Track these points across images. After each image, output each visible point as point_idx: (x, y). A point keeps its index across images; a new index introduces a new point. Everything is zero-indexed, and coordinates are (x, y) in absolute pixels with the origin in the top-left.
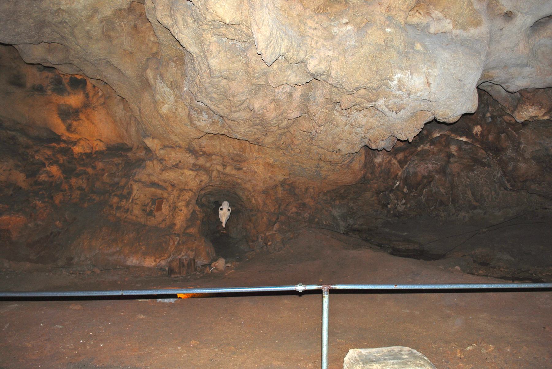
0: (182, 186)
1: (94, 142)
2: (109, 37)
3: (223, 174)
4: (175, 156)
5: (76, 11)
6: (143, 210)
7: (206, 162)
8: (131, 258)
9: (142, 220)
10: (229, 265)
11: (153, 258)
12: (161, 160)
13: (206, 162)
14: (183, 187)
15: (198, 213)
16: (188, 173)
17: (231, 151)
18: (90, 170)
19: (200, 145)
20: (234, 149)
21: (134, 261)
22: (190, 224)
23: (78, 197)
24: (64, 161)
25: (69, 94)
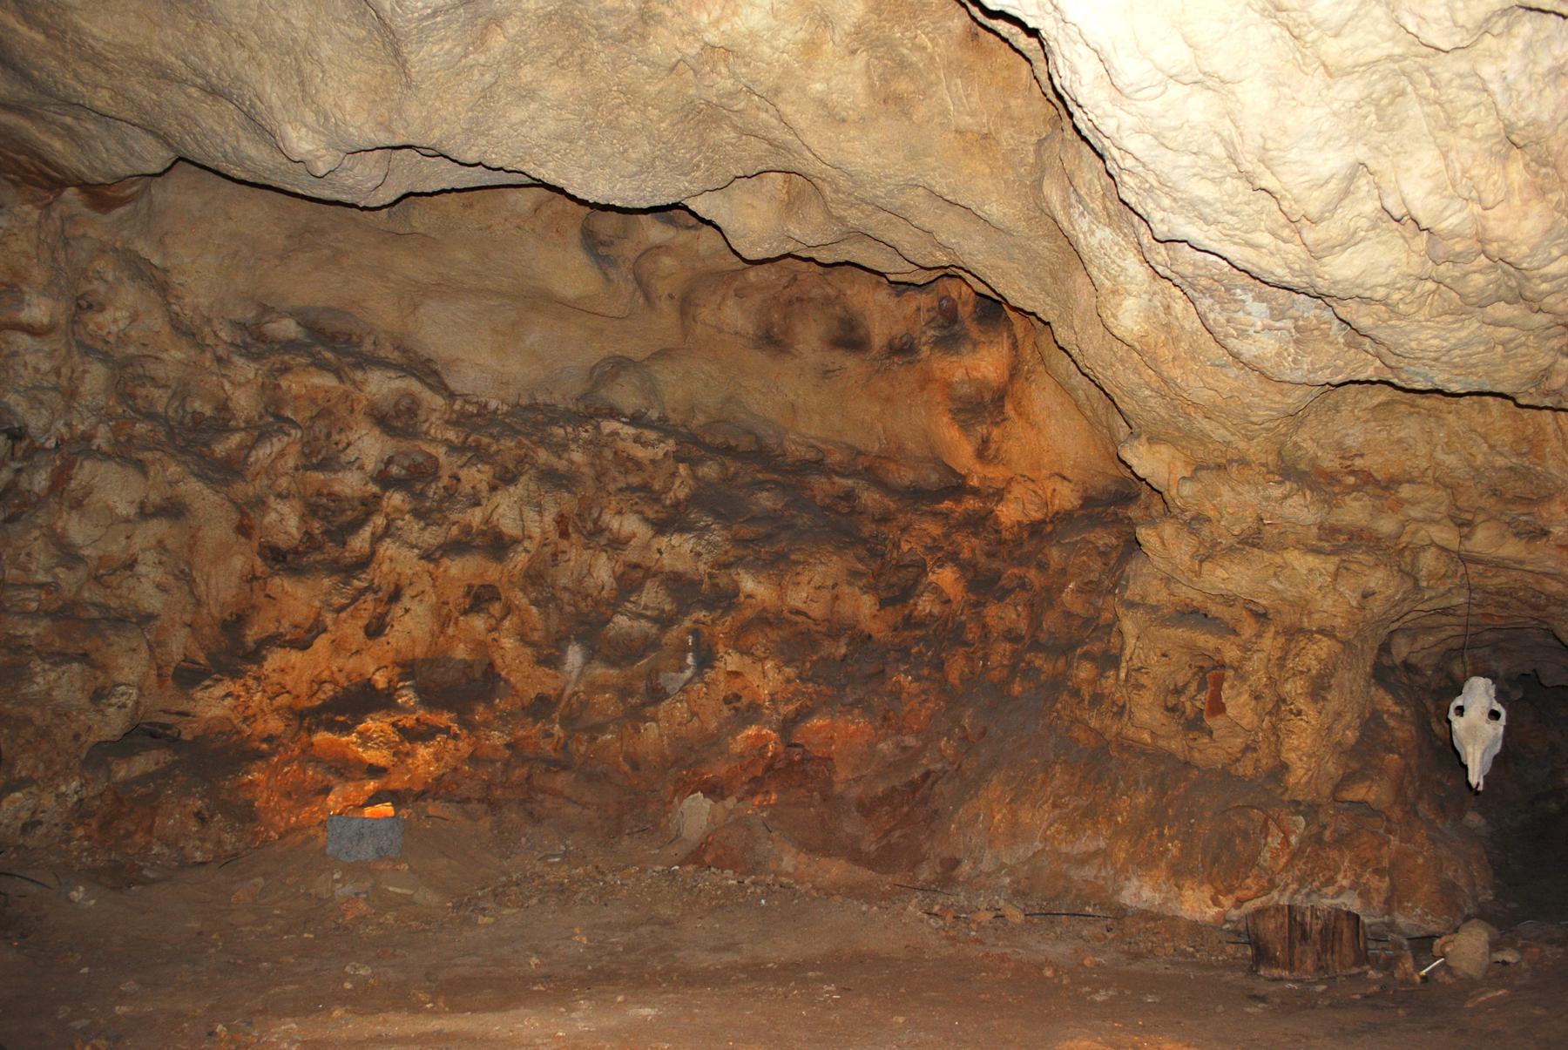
0: (1290, 619)
1: (1046, 483)
2: (898, 99)
3: (1466, 559)
4: (1235, 502)
5: (753, 35)
6: (1172, 710)
7: (1377, 512)
8: (1135, 882)
9: (1175, 745)
10: (1510, 956)
11: (1207, 891)
12: (1195, 522)
13: (1377, 512)
14: (1294, 618)
15: (1392, 723)
16: (1301, 562)
17: (1480, 459)
18: (1032, 575)
19: (1339, 445)
20: (1491, 447)
21: (1146, 893)
22: (1355, 765)
23: (1006, 662)
24: (973, 550)
25: (975, 345)
